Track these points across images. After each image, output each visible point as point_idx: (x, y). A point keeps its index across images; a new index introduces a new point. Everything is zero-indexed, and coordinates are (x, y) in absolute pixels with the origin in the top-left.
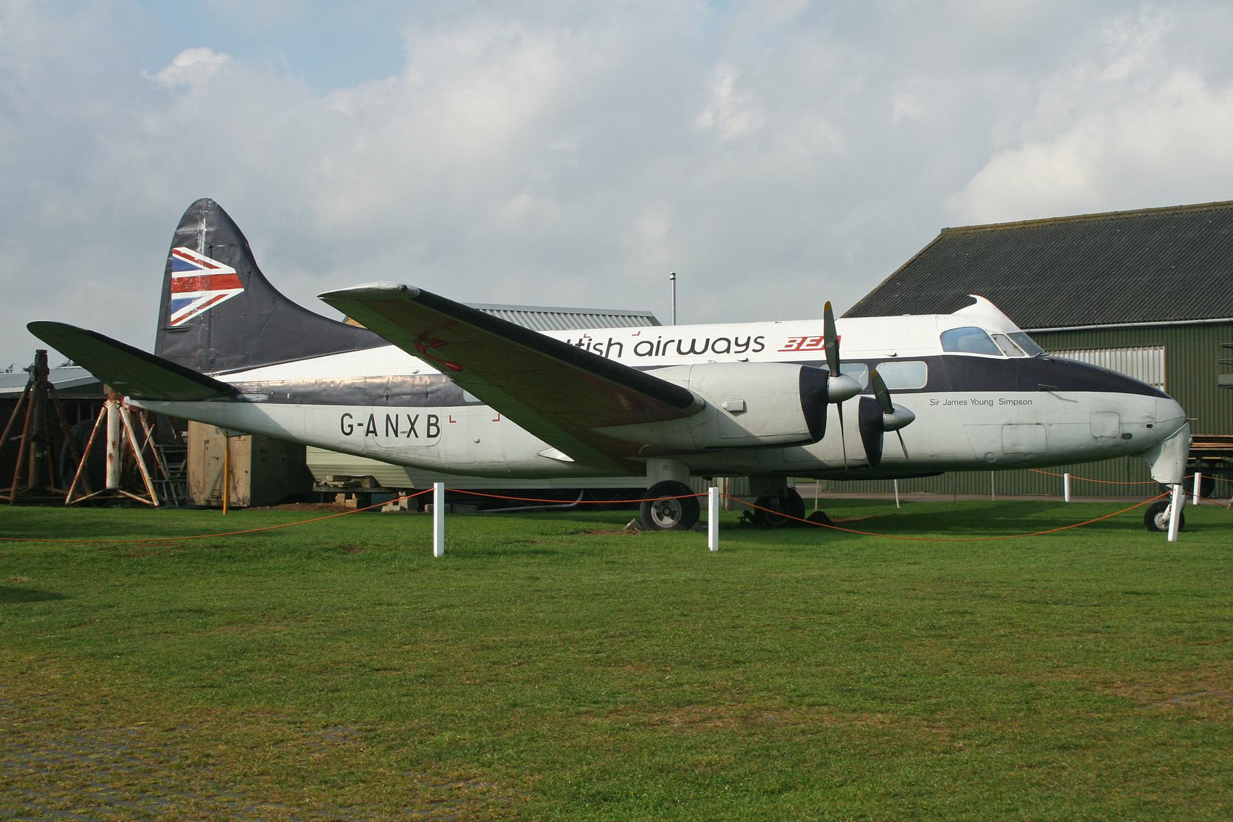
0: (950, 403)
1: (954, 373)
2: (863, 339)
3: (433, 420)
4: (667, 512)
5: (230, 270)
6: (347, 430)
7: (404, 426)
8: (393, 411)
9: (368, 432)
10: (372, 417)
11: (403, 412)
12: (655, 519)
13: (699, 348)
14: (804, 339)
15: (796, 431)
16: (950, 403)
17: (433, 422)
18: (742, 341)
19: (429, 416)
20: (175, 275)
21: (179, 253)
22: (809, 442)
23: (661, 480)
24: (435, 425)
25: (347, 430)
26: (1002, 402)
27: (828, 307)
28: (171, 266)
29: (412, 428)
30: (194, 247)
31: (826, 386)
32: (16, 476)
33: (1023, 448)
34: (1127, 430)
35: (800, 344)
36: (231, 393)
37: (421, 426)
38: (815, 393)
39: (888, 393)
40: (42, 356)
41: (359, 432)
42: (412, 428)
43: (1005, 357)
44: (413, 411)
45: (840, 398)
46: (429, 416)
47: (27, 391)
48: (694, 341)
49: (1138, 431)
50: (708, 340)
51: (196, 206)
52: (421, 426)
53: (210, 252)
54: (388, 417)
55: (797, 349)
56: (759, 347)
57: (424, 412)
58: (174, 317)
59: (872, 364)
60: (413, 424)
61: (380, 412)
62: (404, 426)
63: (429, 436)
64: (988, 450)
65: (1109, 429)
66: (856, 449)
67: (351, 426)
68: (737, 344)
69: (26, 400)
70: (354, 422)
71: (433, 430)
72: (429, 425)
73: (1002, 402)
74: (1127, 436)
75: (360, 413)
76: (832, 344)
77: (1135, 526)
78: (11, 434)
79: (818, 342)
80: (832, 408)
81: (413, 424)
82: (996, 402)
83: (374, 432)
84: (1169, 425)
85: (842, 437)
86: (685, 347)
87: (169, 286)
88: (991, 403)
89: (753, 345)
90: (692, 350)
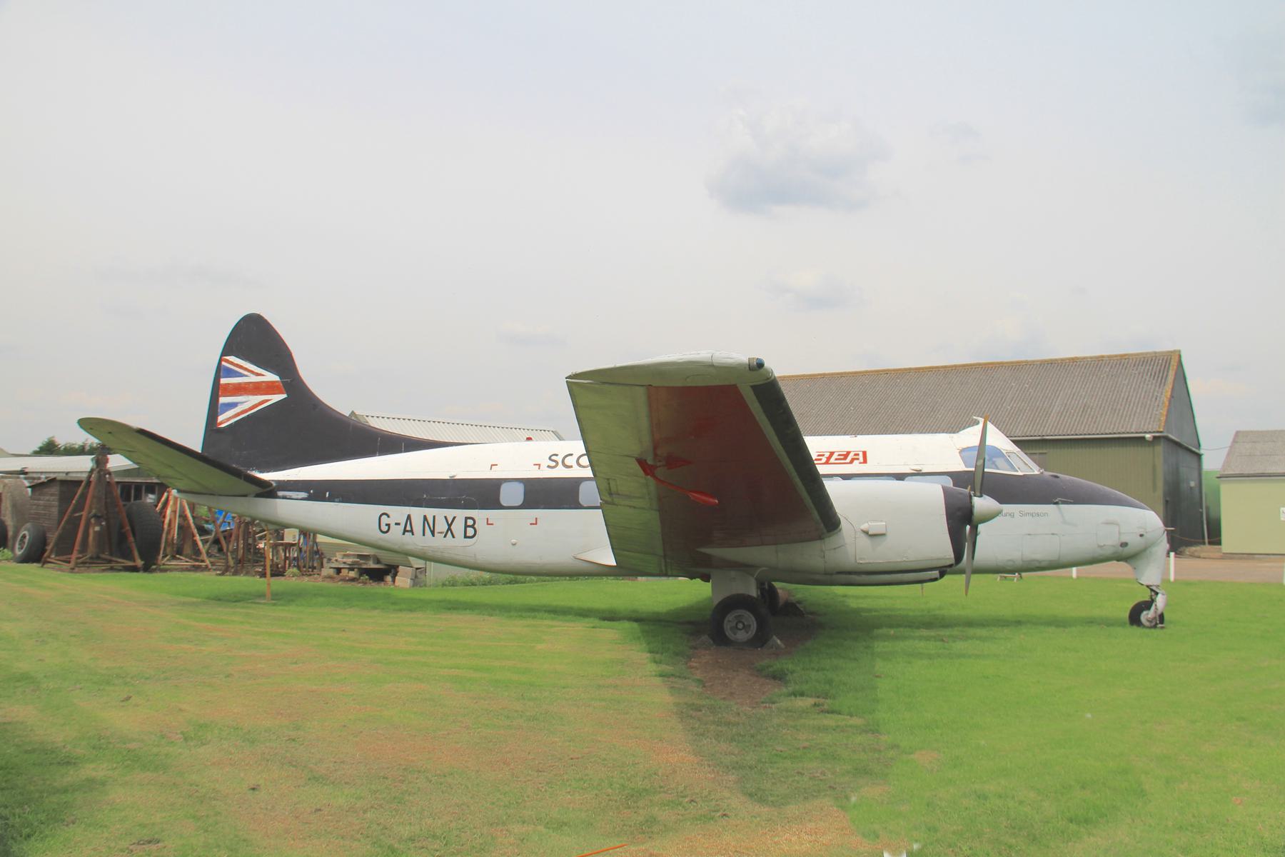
3: (470, 522)
4: (740, 626)
5: (275, 378)
6: (385, 528)
7: (441, 526)
8: (430, 512)
9: (405, 531)
10: (409, 517)
11: (440, 513)
12: (729, 633)
14: (832, 453)
17: (470, 524)
19: (467, 518)
20: (223, 381)
21: (227, 361)
23: (734, 592)
24: (472, 526)
25: (385, 528)
28: (220, 371)
29: (449, 529)
32: (77, 547)
33: (1039, 562)
34: (1124, 539)
35: (829, 458)
36: (268, 491)
37: (458, 527)
41: (396, 532)
42: (449, 529)
43: (1020, 473)
44: (450, 513)
46: (467, 518)
47: (90, 477)
49: (1135, 542)
52: (458, 527)
54: (425, 518)
55: (827, 463)
57: (460, 514)
58: (220, 418)
60: (450, 526)
61: (417, 513)
62: (441, 526)
63: (466, 537)
65: (1110, 541)
67: (388, 525)
69: (89, 483)
70: (392, 521)
71: (470, 532)
72: (466, 526)
73: (1023, 514)
74: (1124, 545)
75: (398, 513)
77: (1122, 624)
78: (75, 511)
81: (450, 526)
82: (1017, 515)
83: (412, 531)
87: (217, 390)
88: (1012, 515)
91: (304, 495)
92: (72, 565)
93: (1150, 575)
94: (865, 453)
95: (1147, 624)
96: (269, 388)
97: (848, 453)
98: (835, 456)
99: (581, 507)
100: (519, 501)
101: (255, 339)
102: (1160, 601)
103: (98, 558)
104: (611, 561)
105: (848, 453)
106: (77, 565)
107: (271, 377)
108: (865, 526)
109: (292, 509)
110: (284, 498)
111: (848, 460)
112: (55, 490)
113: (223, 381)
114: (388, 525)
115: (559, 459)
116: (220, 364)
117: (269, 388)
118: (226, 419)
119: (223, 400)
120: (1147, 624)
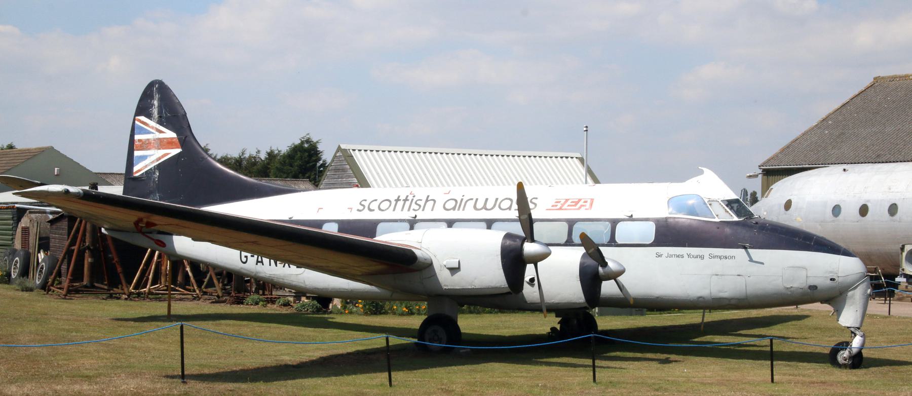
0: (671, 256)
1: (669, 235)
6: (244, 259)
13: (489, 206)
14: (567, 200)
15: (498, 285)
16: (671, 256)
21: (139, 121)
25: (244, 259)
30: (149, 116)
35: (563, 205)
43: (717, 220)
48: (487, 200)
50: (497, 199)
51: (151, 85)
53: (160, 122)
55: (560, 209)
58: (135, 169)
64: (699, 294)
65: (799, 282)
73: (712, 257)
82: (707, 257)
84: (849, 279)
86: (480, 205)
88: (702, 257)
90: (485, 208)
92: (64, 292)
93: (849, 317)
94: (592, 200)
96: (168, 144)
97: (580, 200)
98: (569, 203)
100: (651, 238)
101: (160, 102)
102: (856, 342)
103: (94, 287)
105: (580, 200)
106: (69, 292)
107: (170, 134)
108: (445, 263)
111: (579, 205)
112: (64, 224)
113: (137, 137)
114: (246, 257)
115: (366, 204)
117: (168, 144)
118: (139, 169)
119: (137, 153)
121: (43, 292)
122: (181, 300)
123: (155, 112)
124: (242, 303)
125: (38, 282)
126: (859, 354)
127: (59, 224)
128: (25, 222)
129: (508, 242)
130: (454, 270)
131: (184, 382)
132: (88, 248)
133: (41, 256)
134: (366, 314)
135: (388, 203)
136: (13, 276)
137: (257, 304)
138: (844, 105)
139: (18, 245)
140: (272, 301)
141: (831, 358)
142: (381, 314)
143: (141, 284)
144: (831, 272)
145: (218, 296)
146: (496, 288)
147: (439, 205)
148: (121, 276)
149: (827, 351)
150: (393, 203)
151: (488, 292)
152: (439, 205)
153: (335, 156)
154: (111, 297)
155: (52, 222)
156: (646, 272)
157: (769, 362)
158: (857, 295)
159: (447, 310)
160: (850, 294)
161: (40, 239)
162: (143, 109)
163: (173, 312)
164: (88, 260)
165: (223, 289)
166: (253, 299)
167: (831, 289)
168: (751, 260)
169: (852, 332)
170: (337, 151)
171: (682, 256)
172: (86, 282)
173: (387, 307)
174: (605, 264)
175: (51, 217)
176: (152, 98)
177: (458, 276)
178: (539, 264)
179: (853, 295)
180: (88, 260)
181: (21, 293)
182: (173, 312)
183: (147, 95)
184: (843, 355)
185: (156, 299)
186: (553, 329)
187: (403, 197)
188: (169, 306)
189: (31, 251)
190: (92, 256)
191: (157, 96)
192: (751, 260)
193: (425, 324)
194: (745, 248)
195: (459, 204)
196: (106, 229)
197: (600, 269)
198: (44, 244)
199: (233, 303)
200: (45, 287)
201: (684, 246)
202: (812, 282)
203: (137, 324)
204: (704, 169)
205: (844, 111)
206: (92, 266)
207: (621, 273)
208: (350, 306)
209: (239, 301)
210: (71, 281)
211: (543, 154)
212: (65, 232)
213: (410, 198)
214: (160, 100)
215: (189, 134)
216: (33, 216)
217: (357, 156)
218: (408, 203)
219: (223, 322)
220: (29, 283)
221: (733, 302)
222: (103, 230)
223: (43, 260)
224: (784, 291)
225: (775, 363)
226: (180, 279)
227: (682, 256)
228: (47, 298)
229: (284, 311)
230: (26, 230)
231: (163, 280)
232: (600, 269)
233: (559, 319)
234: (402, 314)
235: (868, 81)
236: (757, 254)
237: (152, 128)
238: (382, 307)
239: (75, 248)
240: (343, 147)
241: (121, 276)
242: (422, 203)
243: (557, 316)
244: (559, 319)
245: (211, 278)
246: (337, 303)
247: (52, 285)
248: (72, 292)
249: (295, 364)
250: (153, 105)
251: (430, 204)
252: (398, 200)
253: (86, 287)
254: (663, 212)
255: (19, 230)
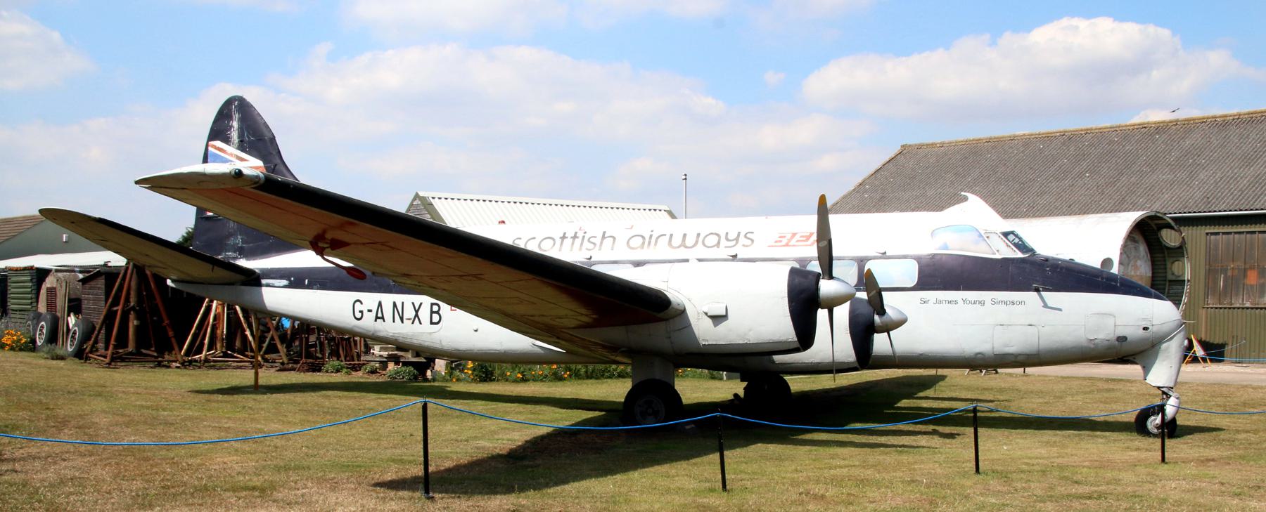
0: (941, 302)
1: (941, 275)
2: (856, 236)
4: (650, 411)
6: (358, 315)
7: (409, 313)
9: (377, 317)
10: (380, 304)
13: (689, 242)
14: (794, 235)
15: (783, 338)
16: (941, 302)
18: (732, 236)
19: (432, 304)
22: (796, 350)
24: (437, 312)
25: (358, 315)
26: (994, 302)
27: (822, 200)
29: (417, 315)
30: (227, 140)
31: (817, 289)
36: (253, 279)
38: (805, 302)
39: (880, 291)
40: (811, 234)
42: (417, 315)
45: (831, 305)
51: (229, 103)
52: (424, 314)
53: (241, 147)
54: (395, 305)
55: (787, 245)
56: (749, 242)
59: (861, 262)
60: (417, 311)
62: (409, 313)
63: (432, 323)
64: (978, 350)
65: (1104, 333)
66: (844, 348)
68: (727, 239)
72: (432, 312)
73: (994, 302)
74: (1122, 339)
76: (825, 243)
79: (808, 238)
80: (822, 314)
81: (417, 311)
82: (988, 302)
83: (383, 318)
84: (1166, 328)
85: (833, 338)
88: (982, 303)
89: (742, 240)
90: (683, 245)
91: (285, 282)
92: (107, 360)
93: (1161, 373)
95: (1155, 431)
99: (853, 259)
100: (913, 281)
101: (239, 122)
104: (787, 378)
106: (113, 359)
109: (277, 298)
110: (268, 285)
112: (101, 282)
116: (207, 149)
120: (1155, 431)
121: (77, 360)
122: (240, 368)
123: (235, 135)
124: (319, 370)
125: (70, 350)
126: (1174, 420)
127: (93, 283)
128: (49, 282)
129: (797, 280)
130: (718, 319)
131: (429, 498)
132: (133, 308)
133: (72, 320)
134: (474, 381)
135: (551, 242)
136: (39, 343)
137: (338, 371)
138: (877, 171)
139: (42, 307)
140: (356, 368)
141: (1139, 426)
142: (492, 380)
143: (196, 348)
144: (1144, 320)
145: (283, 364)
146: (785, 342)
147: (621, 242)
148: (173, 340)
149: (1131, 418)
150: (558, 241)
151: (745, 350)
152: (621, 242)
153: (411, 205)
154: (160, 365)
155: (84, 281)
156: (929, 324)
157: (972, 430)
158: (1173, 348)
159: (657, 373)
160: (1164, 346)
161: (70, 301)
162: (218, 132)
163: (261, 382)
164: (133, 323)
165: (288, 355)
166: (333, 366)
167: (1143, 340)
168: (1046, 306)
169: (1164, 393)
170: (415, 199)
171: (956, 302)
172: (131, 348)
173: (497, 372)
174: (882, 312)
175: (81, 276)
176: (230, 118)
177: (723, 326)
178: (835, 309)
179: (1168, 348)
180: (133, 323)
181: (54, 362)
182: (261, 382)
183: (223, 115)
184: (1154, 422)
185: (211, 367)
186: (736, 395)
187: (570, 234)
188: (257, 374)
189: (59, 314)
190: (138, 318)
191: (236, 116)
192: (1046, 306)
193: (631, 395)
194: (1037, 290)
195: (647, 241)
196: (173, 281)
197: (877, 318)
198: (75, 306)
199: (308, 371)
200: (80, 354)
201: (958, 289)
202: (1121, 332)
203: (226, 397)
204: (969, 195)
205: (878, 175)
206: (137, 328)
207: (901, 323)
208: (457, 373)
209: (316, 368)
210: (116, 347)
211: (631, 206)
212: (102, 291)
213: (580, 235)
214: (242, 120)
215: (278, 161)
216: (60, 274)
217: (436, 203)
218: (578, 241)
219: (330, 393)
220: (60, 352)
221: (1020, 359)
222: (169, 282)
223: (75, 325)
224: (1085, 344)
225: (980, 430)
226: (238, 344)
227: (956, 302)
228: (87, 367)
229: (374, 379)
230: (52, 292)
231: (219, 345)
232: (877, 318)
233: (745, 384)
234: (516, 381)
235: (897, 149)
236: (1052, 297)
237: (231, 155)
238: (492, 373)
239: (119, 308)
240: (421, 194)
241: (173, 340)
242: (597, 241)
243: (742, 380)
244: (745, 384)
245: (272, 339)
246: (440, 365)
247: (91, 352)
248: (117, 360)
249: (504, 452)
250: (232, 127)
251: (608, 241)
252: (564, 237)
253: (131, 353)
254: (929, 247)
255: (43, 291)
